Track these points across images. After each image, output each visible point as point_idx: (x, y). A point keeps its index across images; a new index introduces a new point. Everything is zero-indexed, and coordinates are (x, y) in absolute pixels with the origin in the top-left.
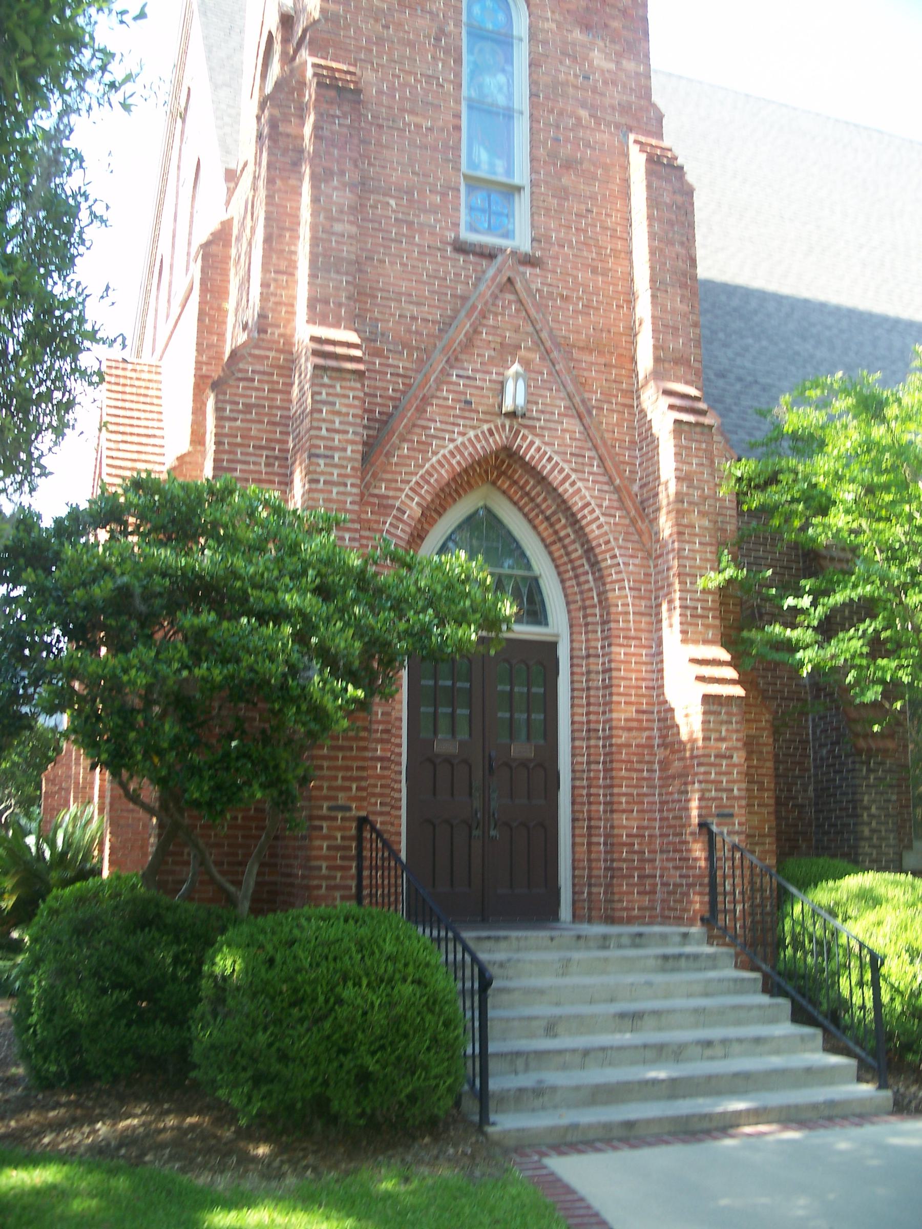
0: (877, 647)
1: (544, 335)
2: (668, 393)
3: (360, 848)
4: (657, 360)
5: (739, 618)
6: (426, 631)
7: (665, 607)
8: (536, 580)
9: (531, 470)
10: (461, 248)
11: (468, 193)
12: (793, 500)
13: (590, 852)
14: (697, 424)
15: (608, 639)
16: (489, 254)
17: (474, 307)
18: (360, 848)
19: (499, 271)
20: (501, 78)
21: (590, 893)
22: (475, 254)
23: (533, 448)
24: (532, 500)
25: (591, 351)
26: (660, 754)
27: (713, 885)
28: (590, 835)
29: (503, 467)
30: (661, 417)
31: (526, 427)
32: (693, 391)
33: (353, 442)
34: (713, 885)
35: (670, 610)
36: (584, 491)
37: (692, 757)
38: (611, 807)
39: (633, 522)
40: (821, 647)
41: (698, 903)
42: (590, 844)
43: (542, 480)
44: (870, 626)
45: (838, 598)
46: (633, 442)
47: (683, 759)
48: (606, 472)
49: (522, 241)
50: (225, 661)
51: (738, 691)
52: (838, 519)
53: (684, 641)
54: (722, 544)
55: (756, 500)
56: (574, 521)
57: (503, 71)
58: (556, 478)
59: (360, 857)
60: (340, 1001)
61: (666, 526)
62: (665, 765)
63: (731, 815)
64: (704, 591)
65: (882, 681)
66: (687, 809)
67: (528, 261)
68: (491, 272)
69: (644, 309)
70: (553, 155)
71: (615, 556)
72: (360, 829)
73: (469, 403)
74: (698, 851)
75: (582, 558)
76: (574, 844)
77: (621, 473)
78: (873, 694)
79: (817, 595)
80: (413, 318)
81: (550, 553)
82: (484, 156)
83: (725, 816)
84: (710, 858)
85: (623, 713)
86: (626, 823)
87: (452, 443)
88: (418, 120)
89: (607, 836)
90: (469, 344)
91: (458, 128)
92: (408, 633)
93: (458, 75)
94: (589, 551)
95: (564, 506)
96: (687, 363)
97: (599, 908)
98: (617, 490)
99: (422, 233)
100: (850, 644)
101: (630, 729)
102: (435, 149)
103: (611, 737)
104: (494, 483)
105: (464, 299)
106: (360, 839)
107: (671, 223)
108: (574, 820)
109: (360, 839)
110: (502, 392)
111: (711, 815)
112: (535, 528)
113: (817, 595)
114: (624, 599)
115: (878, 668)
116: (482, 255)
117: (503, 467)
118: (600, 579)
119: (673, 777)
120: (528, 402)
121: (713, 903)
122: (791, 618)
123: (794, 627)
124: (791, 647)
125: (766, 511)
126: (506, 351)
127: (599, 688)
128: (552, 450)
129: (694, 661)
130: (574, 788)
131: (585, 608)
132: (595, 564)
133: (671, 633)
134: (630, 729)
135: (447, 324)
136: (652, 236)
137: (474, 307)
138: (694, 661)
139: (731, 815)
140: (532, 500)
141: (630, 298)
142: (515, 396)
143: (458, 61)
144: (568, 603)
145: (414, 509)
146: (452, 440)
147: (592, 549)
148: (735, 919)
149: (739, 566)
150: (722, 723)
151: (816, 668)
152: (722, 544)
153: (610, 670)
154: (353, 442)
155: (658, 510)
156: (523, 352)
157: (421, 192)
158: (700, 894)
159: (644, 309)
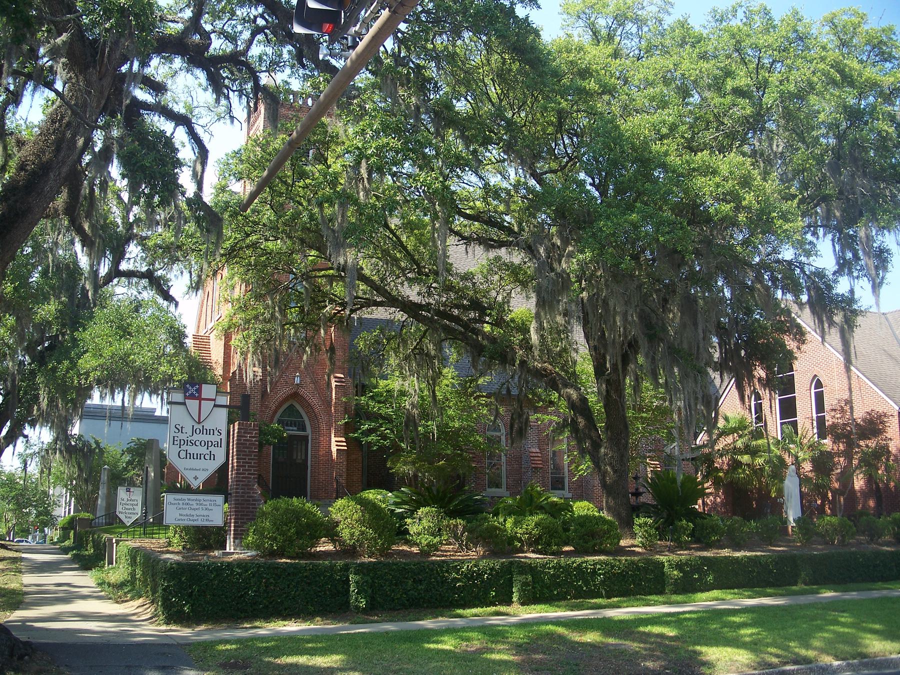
2: (336, 377)
23: (302, 391)
29: (295, 395)
32: (342, 376)
36: (315, 401)
75: (314, 418)
114: (323, 426)
127: (316, 447)
142: (297, 380)
145: (274, 407)
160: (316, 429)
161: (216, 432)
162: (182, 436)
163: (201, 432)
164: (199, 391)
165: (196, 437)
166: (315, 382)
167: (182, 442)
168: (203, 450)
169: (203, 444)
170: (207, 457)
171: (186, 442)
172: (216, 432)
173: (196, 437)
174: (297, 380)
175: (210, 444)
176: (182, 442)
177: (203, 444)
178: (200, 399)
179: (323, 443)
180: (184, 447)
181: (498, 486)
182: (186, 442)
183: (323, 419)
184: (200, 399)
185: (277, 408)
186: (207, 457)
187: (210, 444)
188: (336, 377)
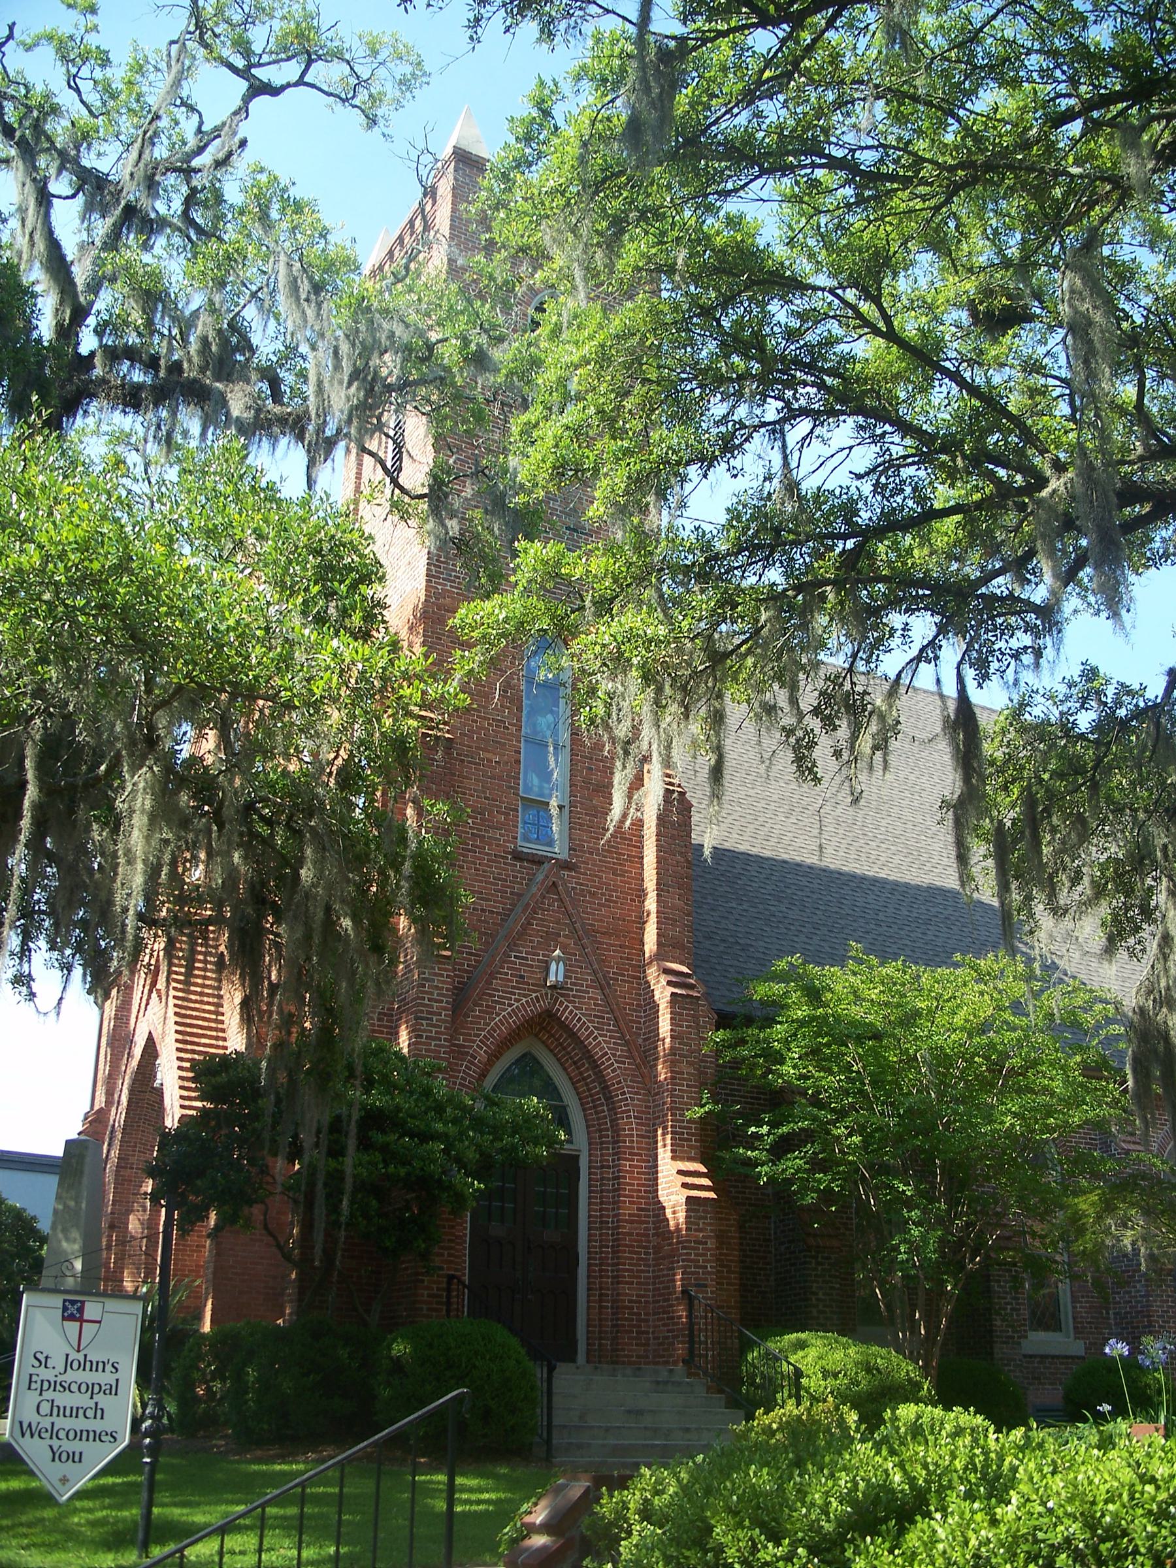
0: (817, 1165)
1: (578, 925)
2: (667, 971)
3: (449, 1297)
4: (659, 944)
5: (712, 1144)
6: (514, 1148)
7: (660, 1132)
8: (564, 1108)
9: (565, 1027)
10: (518, 856)
11: (524, 810)
12: (756, 1056)
13: (600, 1313)
14: (688, 996)
15: (617, 1154)
16: (538, 861)
17: (528, 905)
18: (449, 1297)
19: (547, 876)
20: (550, 717)
21: (600, 1345)
22: (528, 861)
23: (567, 1011)
24: (564, 1049)
25: (611, 935)
26: (654, 1241)
27: (691, 1335)
28: (601, 1301)
29: (545, 1024)
30: (662, 993)
31: (562, 995)
32: (685, 970)
33: (445, 1009)
34: (691, 1335)
35: (663, 1134)
36: (604, 1045)
37: (678, 1243)
38: (617, 1280)
39: (638, 1067)
40: (774, 1164)
41: (681, 1349)
42: (601, 1307)
43: (573, 1035)
44: (809, 1149)
45: (784, 1129)
46: (639, 1005)
47: (671, 1244)
48: (620, 1030)
49: (560, 849)
50: (404, 1164)
51: (712, 1195)
52: (787, 1069)
53: (673, 1158)
54: (702, 1084)
55: (728, 1055)
56: (595, 1065)
57: (552, 712)
58: (583, 1033)
59: (449, 1303)
60: (474, 1367)
61: (662, 1072)
62: (657, 1249)
63: (705, 1286)
64: (689, 1121)
65: (818, 1191)
66: (674, 1281)
67: (566, 866)
68: (540, 877)
69: (651, 904)
70: (587, 781)
71: (623, 1093)
72: (449, 1283)
73: (522, 977)
74: (682, 1312)
75: (600, 1095)
76: (589, 1308)
77: (630, 1028)
78: (810, 1199)
79: (774, 1125)
80: (483, 911)
81: (576, 1089)
82: (536, 781)
83: (701, 1286)
84: (689, 1317)
85: (628, 1210)
86: (629, 1292)
87: (510, 1007)
88: (489, 756)
89: (613, 1301)
90: (523, 933)
91: (518, 762)
92: (502, 1150)
93: (519, 720)
94: (605, 1088)
95: (588, 1055)
96: (683, 947)
97: (607, 1355)
98: (627, 1043)
99: (490, 845)
100: (794, 1163)
101: (632, 1222)
102: (501, 779)
103: (618, 1227)
104: (536, 1035)
105: (519, 895)
106: (449, 1290)
107: (673, 837)
108: (589, 1289)
109: (449, 1290)
110: (547, 970)
111: (690, 1285)
112: (565, 1069)
113: (774, 1125)
114: (631, 1126)
115: (815, 1180)
116: (533, 862)
117: (545, 1024)
118: (613, 1109)
119: (663, 1258)
120: (565, 977)
121: (691, 1351)
122: (752, 1142)
123: (753, 1149)
124: (753, 1163)
125: (736, 1064)
126: (550, 939)
127: (610, 1189)
128: (580, 1014)
129: (680, 1172)
130: (589, 1265)
131: (600, 1131)
132: (609, 1098)
133: (664, 1155)
134: (632, 1222)
135: (506, 916)
136: (659, 848)
137: (528, 905)
138: (680, 1172)
139: (705, 1286)
140: (564, 1049)
141: (642, 894)
142: (556, 973)
143: (520, 709)
144: (588, 1127)
145: (482, 1055)
146: (510, 1005)
147: (607, 1087)
148: (707, 1363)
149: (716, 1103)
150: (700, 1218)
151: (772, 1180)
152: (702, 1084)
153: (618, 1178)
154: (445, 1009)
155: (657, 1059)
156: (561, 939)
157: (491, 813)
158: (682, 1343)
159: (651, 904)
160: (607, 1133)
161: (109, 1368)
162: (45, 1374)
163: (82, 1366)
164: (81, 1310)
165: (71, 1376)
166: (603, 985)
167: (46, 1385)
168: (83, 1400)
169: (83, 1388)
170: (90, 1413)
171: (53, 1385)
172: (109, 1368)
173: (71, 1376)
174: (556, 973)
175: (97, 1388)
176: (46, 1385)
177: (83, 1388)
178: (81, 1320)
179: (632, 1182)
180: (48, 1395)
181: (1057, 1328)
182: (53, 1385)
183: (629, 1100)
184: (81, 1320)
185: (494, 1057)
186: (90, 1413)
187: (97, 1388)
188: (667, 971)
